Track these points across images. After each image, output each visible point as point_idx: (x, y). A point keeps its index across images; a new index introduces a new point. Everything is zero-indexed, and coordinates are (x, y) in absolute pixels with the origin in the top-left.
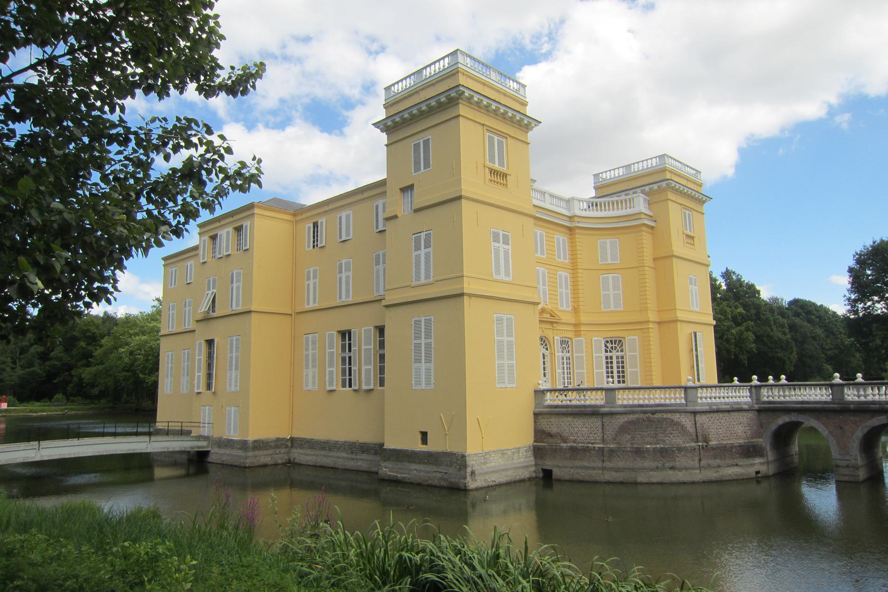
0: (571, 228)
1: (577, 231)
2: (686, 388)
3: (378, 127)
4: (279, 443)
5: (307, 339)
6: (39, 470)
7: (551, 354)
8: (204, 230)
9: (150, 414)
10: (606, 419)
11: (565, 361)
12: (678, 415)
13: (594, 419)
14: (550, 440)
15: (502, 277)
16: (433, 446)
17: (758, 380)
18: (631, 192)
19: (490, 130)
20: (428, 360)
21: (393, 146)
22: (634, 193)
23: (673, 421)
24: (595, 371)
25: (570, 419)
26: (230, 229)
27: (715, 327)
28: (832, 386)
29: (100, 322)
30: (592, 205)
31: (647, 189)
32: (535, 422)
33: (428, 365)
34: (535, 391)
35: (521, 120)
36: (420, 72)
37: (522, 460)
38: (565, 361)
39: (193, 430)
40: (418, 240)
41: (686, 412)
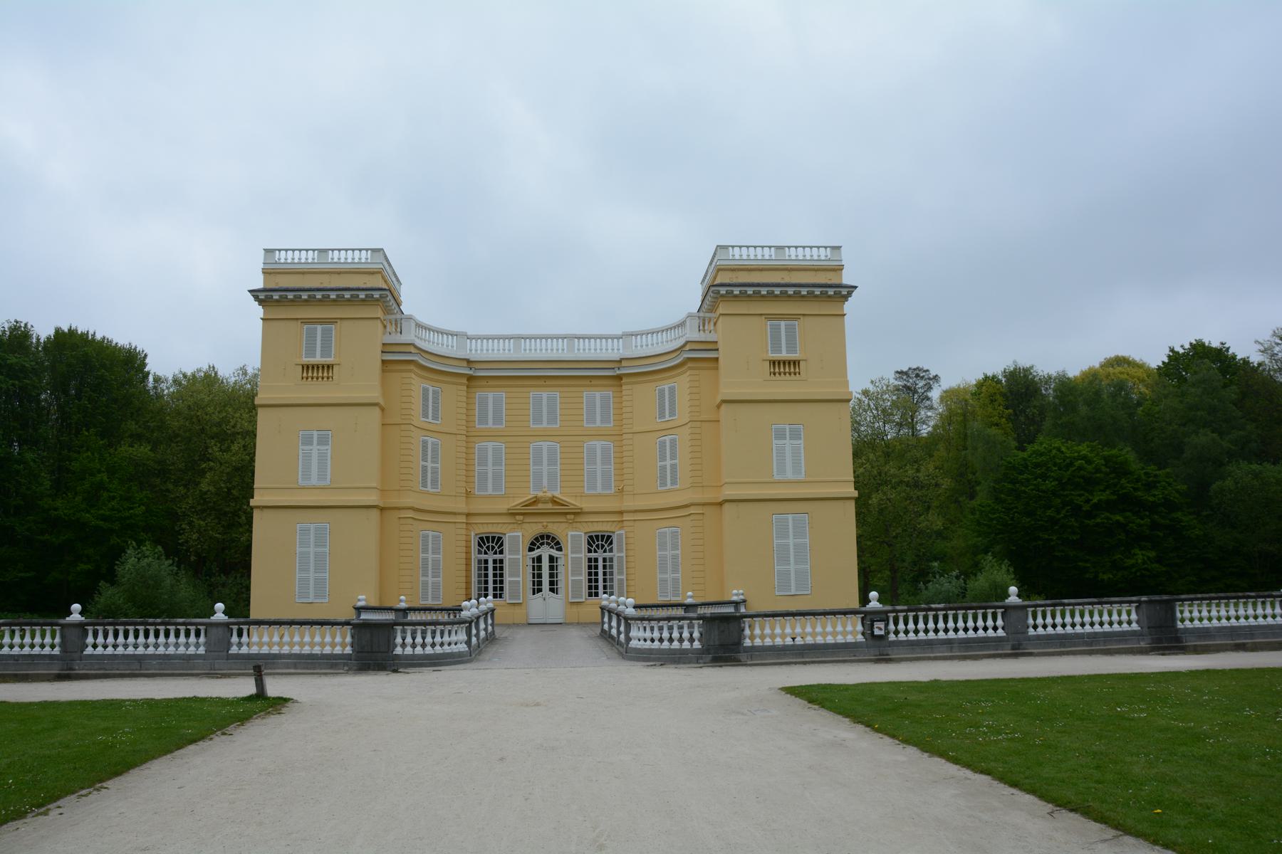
9: (248, 616)
17: (879, 601)
24: (520, 579)
27: (857, 500)
28: (1007, 610)
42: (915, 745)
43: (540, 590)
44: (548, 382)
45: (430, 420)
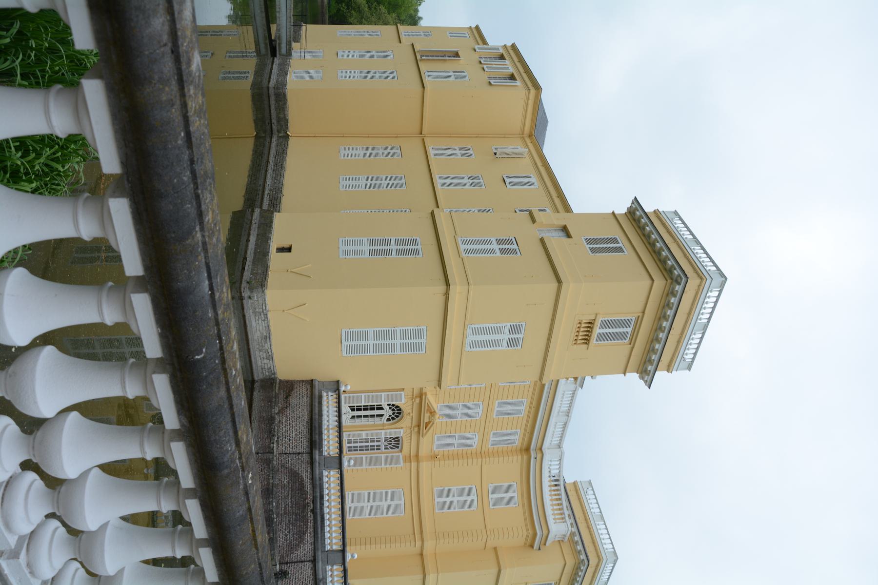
0: (530, 450)
1: (525, 457)
2: (343, 551)
3: (633, 203)
4: (283, 123)
5: (396, 148)
6: (318, 477)
7: (383, 425)
8: (509, 49)
10: (306, 457)
11: (375, 444)
12: (311, 540)
13: (306, 444)
14: (282, 396)
15: (470, 338)
16: (275, 260)
18: (572, 520)
19: (639, 320)
20: (365, 155)
21: (612, 217)
22: (572, 524)
23: (305, 534)
25: (306, 418)
26: (512, 70)
29: (412, 12)
30: (556, 481)
31: (577, 538)
32: (303, 381)
33: (367, 252)
34: (338, 382)
35: (650, 362)
36: (698, 243)
37: (259, 363)
38: (375, 444)
39: (298, 44)
40: (509, 242)
41: (315, 550)
42: (191, 422)
43: (353, 410)
44: (533, 410)
45: (492, 439)
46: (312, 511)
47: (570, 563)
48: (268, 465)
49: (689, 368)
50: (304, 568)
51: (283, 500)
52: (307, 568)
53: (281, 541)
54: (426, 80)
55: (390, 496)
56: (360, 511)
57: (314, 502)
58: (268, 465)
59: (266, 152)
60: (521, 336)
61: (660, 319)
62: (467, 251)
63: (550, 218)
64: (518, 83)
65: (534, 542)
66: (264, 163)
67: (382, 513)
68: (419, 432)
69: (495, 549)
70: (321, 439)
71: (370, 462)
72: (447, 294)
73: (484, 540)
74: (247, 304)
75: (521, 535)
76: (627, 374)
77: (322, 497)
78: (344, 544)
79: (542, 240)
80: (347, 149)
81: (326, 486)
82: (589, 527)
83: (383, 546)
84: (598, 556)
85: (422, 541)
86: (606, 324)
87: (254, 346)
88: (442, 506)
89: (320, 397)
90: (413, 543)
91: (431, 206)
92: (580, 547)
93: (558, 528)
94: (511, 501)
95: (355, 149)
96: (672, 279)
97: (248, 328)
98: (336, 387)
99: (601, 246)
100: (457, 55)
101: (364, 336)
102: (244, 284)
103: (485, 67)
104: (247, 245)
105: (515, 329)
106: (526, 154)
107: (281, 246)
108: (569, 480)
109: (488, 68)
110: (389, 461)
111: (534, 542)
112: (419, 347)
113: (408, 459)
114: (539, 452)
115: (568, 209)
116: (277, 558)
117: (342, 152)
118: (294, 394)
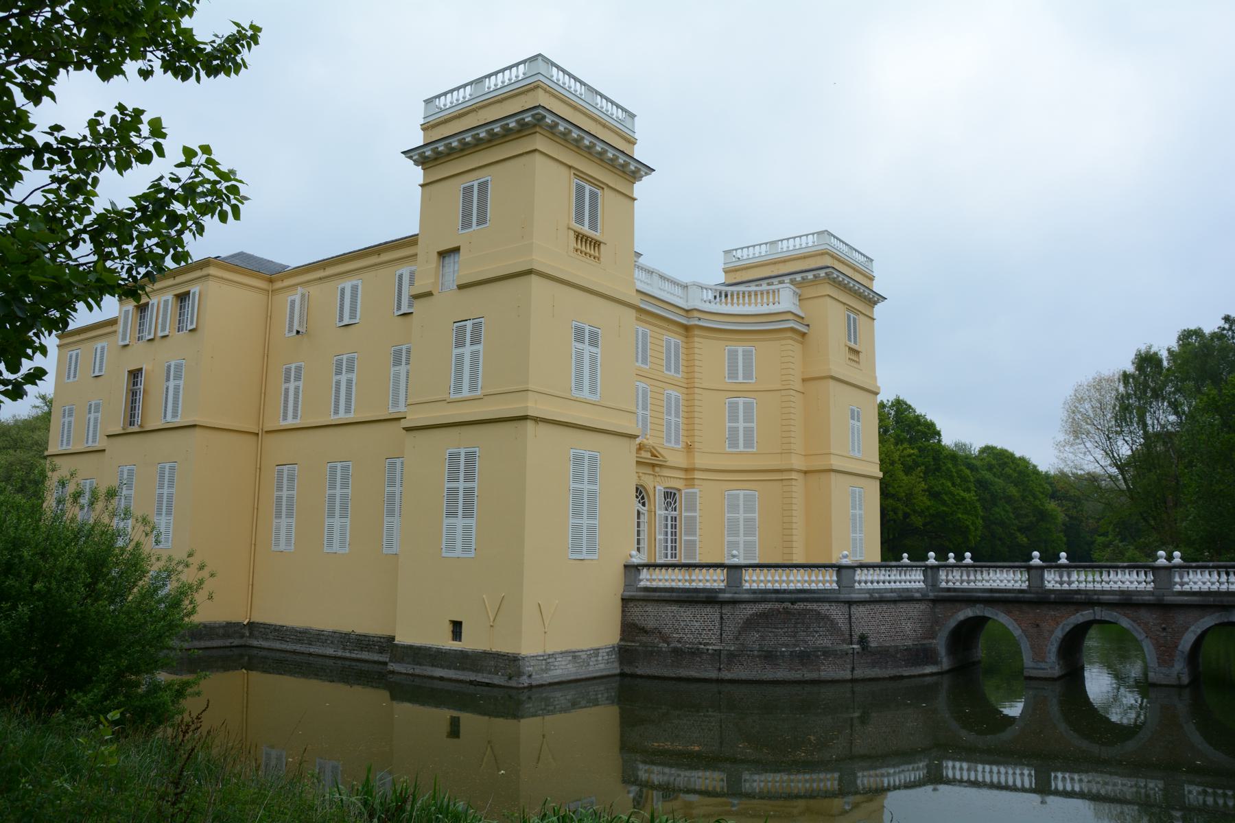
0: (688, 325)
1: (696, 332)
2: (839, 568)
3: (411, 158)
5: (280, 473)
7: (649, 511)
10: (727, 610)
12: (827, 606)
14: (644, 639)
15: (586, 394)
16: (471, 642)
18: (775, 281)
19: (579, 174)
22: (780, 283)
23: (819, 613)
25: (675, 608)
26: (169, 296)
30: (722, 295)
31: (798, 278)
32: (623, 611)
33: (467, 521)
34: (626, 566)
36: (480, 81)
37: (602, 666)
40: (461, 332)
41: (837, 601)
46: (793, 603)
47: (829, 290)
48: (735, 656)
49: (633, 116)
50: (857, 615)
51: (779, 639)
52: (859, 611)
53: (826, 642)
54: (180, 421)
55: (734, 507)
56: (749, 546)
57: (782, 601)
58: (735, 656)
59: (278, 655)
60: (587, 328)
61: (578, 147)
62: (473, 387)
63: (425, 271)
64: (195, 289)
65: (799, 331)
66: (298, 658)
67: (753, 519)
68: (660, 466)
69: (804, 380)
70: (704, 590)
71: (691, 531)
72: (537, 420)
73: (793, 393)
74: (538, 679)
75: (791, 347)
76: (635, 196)
77: (777, 591)
78: (832, 566)
79: (461, 287)
80: (277, 540)
81: (762, 586)
82: (785, 261)
83: (794, 520)
84: (822, 254)
85: (791, 470)
86: (579, 218)
87: (584, 673)
88: (748, 442)
89: (646, 589)
90: (794, 483)
91: (396, 428)
92: (810, 276)
93: (785, 300)
94: (747, 355)
95: (278, 529)
96: (535, 126)
97: (563, 679)
98: (632, 569)
99: (475, 209)
100: (135, 374)
101: (577, 528)
102: (513, 683)
103: (160, 334)
104: (450, 680)
105: (579, 337)
106: (305, 291)
107: (450, 635)
108: (722, 278)
109: (163, 329)
110: (691, 507)
111: (799, 331)
112: (470, 457)
113: (690, 482)
114: (690, 315)
115: (410, 241)
116: (845, 647)
117: (282, 547)
118: (641, 622)
